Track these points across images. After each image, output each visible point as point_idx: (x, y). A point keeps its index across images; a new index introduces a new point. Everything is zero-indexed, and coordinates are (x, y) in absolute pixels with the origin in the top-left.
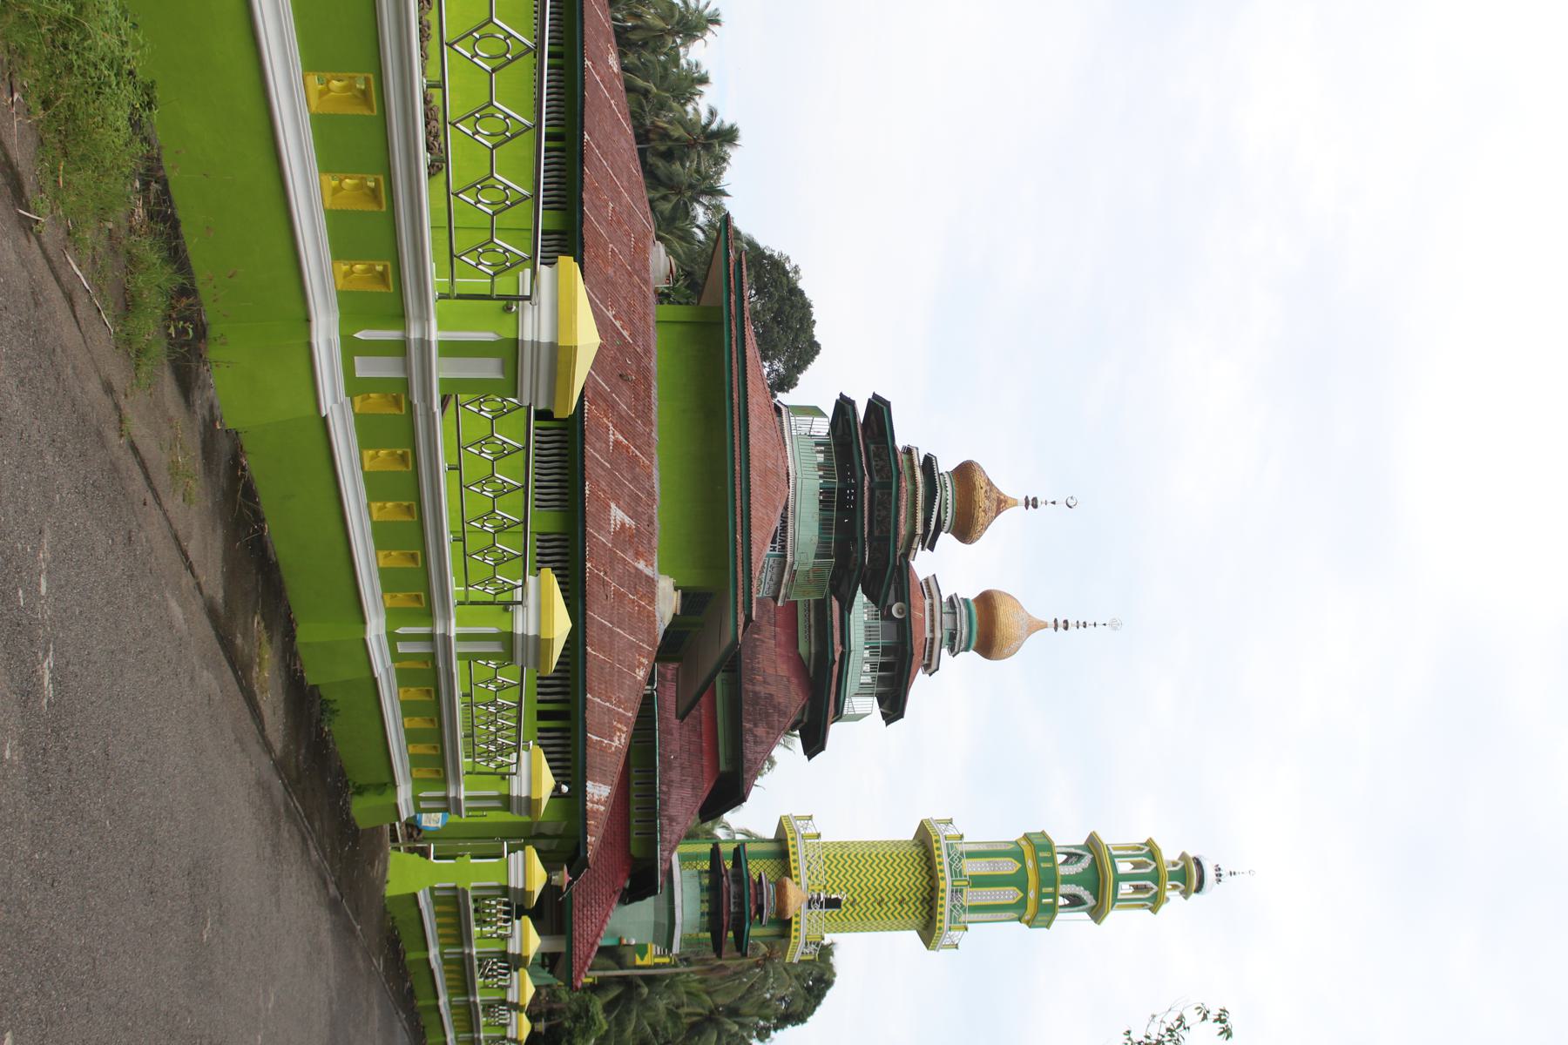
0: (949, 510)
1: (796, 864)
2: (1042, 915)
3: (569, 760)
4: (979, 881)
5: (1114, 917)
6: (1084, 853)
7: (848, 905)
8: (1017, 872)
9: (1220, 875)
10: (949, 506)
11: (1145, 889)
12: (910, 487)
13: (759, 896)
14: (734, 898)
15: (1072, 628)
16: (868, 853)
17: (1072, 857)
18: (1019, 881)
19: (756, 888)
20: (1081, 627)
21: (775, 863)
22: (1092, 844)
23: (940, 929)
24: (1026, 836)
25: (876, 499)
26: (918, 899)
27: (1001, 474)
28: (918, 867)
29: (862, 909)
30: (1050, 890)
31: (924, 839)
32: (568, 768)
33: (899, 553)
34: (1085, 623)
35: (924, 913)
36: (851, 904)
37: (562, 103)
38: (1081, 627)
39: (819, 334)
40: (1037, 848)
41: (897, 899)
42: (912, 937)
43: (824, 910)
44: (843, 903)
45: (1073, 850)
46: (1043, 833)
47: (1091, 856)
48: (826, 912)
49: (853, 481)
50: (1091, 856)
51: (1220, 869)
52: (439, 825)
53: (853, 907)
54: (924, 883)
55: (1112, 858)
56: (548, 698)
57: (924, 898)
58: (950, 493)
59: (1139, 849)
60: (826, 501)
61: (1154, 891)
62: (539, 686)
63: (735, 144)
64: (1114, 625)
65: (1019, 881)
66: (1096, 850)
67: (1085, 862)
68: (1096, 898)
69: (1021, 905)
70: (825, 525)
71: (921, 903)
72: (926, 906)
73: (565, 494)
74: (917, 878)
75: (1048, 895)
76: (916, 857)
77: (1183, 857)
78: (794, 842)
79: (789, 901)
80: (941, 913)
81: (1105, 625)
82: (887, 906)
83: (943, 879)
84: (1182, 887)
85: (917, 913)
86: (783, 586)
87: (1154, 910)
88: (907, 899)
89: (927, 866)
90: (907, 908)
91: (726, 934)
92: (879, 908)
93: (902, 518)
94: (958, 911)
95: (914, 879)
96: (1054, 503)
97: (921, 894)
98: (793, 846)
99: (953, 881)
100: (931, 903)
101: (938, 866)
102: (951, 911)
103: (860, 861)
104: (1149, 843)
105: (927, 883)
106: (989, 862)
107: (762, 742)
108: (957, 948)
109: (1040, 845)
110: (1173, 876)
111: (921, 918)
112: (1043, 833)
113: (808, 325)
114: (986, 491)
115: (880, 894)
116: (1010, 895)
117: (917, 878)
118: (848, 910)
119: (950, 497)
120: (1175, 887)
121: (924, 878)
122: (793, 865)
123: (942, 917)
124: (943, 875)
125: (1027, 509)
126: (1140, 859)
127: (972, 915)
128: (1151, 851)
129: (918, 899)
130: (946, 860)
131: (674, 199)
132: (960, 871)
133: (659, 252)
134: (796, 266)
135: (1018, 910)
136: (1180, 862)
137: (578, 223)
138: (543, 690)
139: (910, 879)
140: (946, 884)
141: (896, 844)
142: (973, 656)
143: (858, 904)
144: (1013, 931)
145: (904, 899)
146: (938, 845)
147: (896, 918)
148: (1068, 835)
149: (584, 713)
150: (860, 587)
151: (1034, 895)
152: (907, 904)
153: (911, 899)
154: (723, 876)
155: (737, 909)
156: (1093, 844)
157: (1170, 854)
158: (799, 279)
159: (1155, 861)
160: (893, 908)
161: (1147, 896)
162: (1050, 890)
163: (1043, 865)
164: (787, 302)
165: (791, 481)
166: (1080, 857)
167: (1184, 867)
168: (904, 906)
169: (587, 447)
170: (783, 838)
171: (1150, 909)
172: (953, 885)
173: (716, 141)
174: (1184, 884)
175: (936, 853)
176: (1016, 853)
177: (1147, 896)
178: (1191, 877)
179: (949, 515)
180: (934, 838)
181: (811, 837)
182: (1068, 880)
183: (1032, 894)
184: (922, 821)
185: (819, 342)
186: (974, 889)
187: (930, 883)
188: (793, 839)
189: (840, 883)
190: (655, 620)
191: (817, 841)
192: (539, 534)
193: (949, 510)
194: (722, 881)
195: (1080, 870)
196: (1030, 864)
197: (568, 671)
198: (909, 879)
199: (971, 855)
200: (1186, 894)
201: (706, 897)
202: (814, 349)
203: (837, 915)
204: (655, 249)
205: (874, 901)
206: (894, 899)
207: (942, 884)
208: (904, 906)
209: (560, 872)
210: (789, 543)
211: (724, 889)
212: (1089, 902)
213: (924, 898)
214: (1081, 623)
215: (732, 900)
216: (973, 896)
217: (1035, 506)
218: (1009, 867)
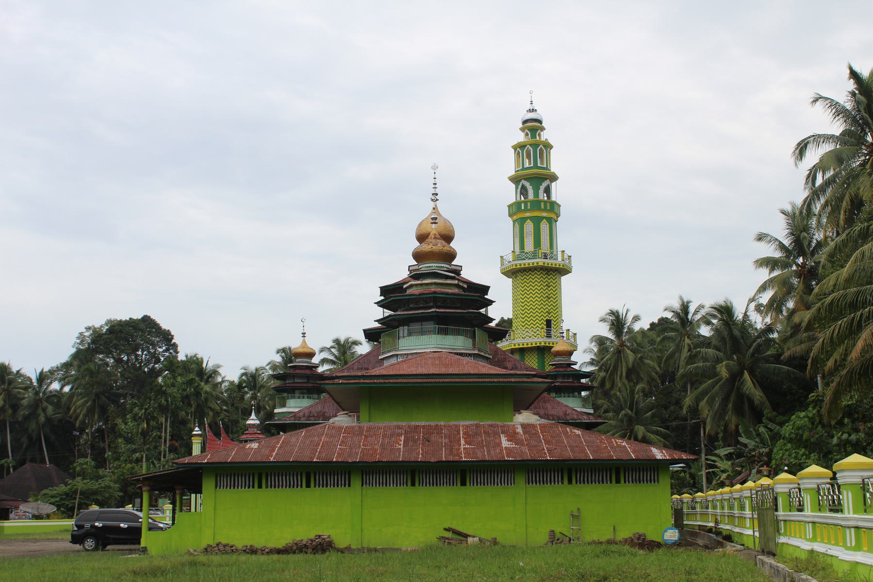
0: (442, 265)
1: (530, 344)
2: (553, 208)
3: (639, 468)
4: (537, 243)
5: (554, 168)
6: (521, 184)
7: (550, 316)
8: (532, 222)
9: (533, 109)
10: (440, 265)
11: (541, 151)
12: (433, 286)
13: (562, 366)
14: (565, 379)
15: (437, 191)
16: (521, 303)
17: (524, 191)
18: (537, 221)
19: (559, 367)
20: (436, 186)
21: (527, 355)
22: (515, 179)
23: (563, 266)
24: (510, 215)
25: (442, 305)
26: (547, 277)
28: (529, 277)
30: (542, 204)
31: (511, 273)
32: (643, 468)
33: (463, 293)
34: (434, 184)
35: (554, 274)
36: (549, 314)
37: (288, 473)
38: (436, 186)
39: (138, 315)
40: (519, 210)
41: (546, 289)
42: (564, 279)
43: (552, 329)
44: (549, 318)
45: (519, 190)
46: (509, 206)
47: (523, 181)
48: (553, 327)
50: (523, 181)
51: (530, 110)
52: (677, 531)
53: (551, 313)
54: (539, 274)
55: (524, 169)
56: (299, 483)
57: (546, 273)
58: (433, 265)
59: (519, 153)
60: (444, 332)
61: (542, 147)
62: (249, 488)
63: (8, 364)
64: (435, 168)
65: (537, 221)
66: (520, 177)
67: (527, 184)
68: (546, 179)
70: (457, 333)
71: (549, 276)
72: (550, 273)
73: (379, 471)
74: (536, 277)
76: (524, 277)
77: (522, 130)
78: (517, 344)
79: (566, 349)
80: (552, 264)
81: (435, 173)
82: (550, 294)
83: (537, 263)
84: (539, 131)
85: (554, 278)
86: (480, 353)
87: (551, 147)
88: (547, 283)
89: (534, 271)
90: (551, 283)
91: (582, 383)
92: (551, 299)
93: (450, 291)
95: (536, 279)
97: (544, 275)
98: (519, 345)
100: (549, 270)
103: (526, 308)
104: (515, 148)
105: (527, 272)
106: (526, 238)
107: (515, 364)
108: (571, 256)
109: (514, 209)
110: (534, 136)
111: (556, 276)
112: (509, 206)
113: (134, 322)
114: (433, 245)
115: (544, 298)
116: (544, 226)
117: (536, 277)
118: (552, 316)
119: (436, 265)
120: (539, 135)
121: (536, 273)
122: (529, 346)
123: (554, 264)
124: (531, 263)
126: (525, 154)
127: (554, 248)
128: (519, 148)
129: (547, 277)
130: (527, 261)
131: (45, 404)
132: (533, 253)
133: (338, 421)
134: (86, 328)
135: (552, 222)
136: (525, 132)
137: (364, 464)
138: (343, 485)
139: (536, 281)
140: (540, 262)
141: (514, 287)
143: (549, 310)
144: (561, 225)
145: (547, 285)
146: (518, 265)
147: (556, 289)
148: (510, 193)
149: (624, 460)
151: (544, 213)
152: (549, 283)
153: (547, 281)
154: (555, 385)
155: (571, 378)
156: (515, 180)
157: (521, 137)
158: (94, 327)
159: (526, 146)
160: (552, 291)
161: (545, 151)
162: (542, 204)
163: (529, 208)
164: (119, 335)
165: (438, 350)
166: (523, 187)
167: (528, 130)
168: (550, 285)
169: (248, 460)
170: (511, 350)
171: (550, 149)
172: (541, 258)
173: (6, 378)
174: (538, 130)
175: (523, 266)
176: (520, 223)
177: (545, 151)
178: (533, 126)
179: (444, 265)
180: (514, 267)
182: (536, 194)
183: (545, 214)
184: (502, 273)
185: (142, 316)
186: (542, 245)
187: (538, 270)
188: (515, 345)
189: (539, 320)
190: (543, 424)
192: (362, 486)
193: (442, 265)
194: (557, 386)
195: (531, 187)
196: (528, 215)
197: (595, 469)
198: (536, 282)
199: (522, 246)
200: (543, 129)
201: (566, 395)
202: (146, 319)
203: (555, 322)
204: (337, 423)
205: (548, 301)
206: (547, 290)
207: (541, 264)
208: (550, 285)
209: (763, 471)
210: (468, 352)
211: (562, 385)
212: (548, 183)
213: (546, 273)
214: (434, 186)
215: (566, 380)
217: (305, 333)
218: (529, 227)
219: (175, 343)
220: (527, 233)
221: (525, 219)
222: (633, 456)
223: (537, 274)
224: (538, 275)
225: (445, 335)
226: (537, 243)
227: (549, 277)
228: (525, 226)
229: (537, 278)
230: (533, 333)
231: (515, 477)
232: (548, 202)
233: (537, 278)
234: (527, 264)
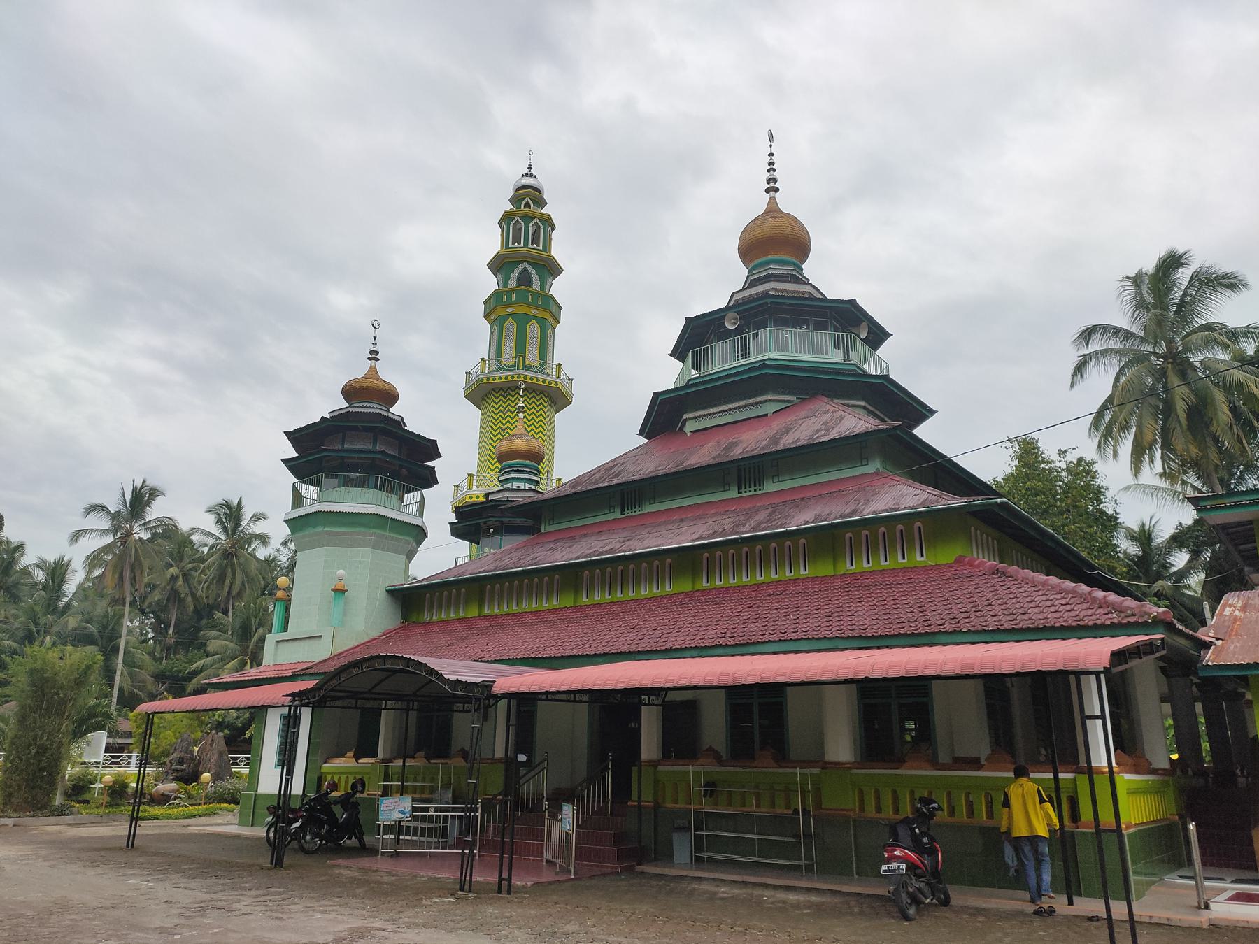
4: (521, 350)
18: (523, 320)
27: (358, 370)
29: (537, 417)
47: (525, 264)
50: (525, 264)
65: (523, 320)
69: (542, 322)
74: (501, 400)
75: (535, 299)
89: (540, 393)
96: (375, 338)
116: (533, 330)
125: (379, 360)
142: (810, 269)
172: (523, 369)
183: (535, 312)
191: (475, 477)
196: (510, 310)
216: (532, 356)
217: (377, 353)
218: (511, 327)
221: (504, 318)
224: (512, 396)
226: (521, 350)
229: (536, 398)
230: (489, 477)
231: (399, 711)
233: (536, 398)
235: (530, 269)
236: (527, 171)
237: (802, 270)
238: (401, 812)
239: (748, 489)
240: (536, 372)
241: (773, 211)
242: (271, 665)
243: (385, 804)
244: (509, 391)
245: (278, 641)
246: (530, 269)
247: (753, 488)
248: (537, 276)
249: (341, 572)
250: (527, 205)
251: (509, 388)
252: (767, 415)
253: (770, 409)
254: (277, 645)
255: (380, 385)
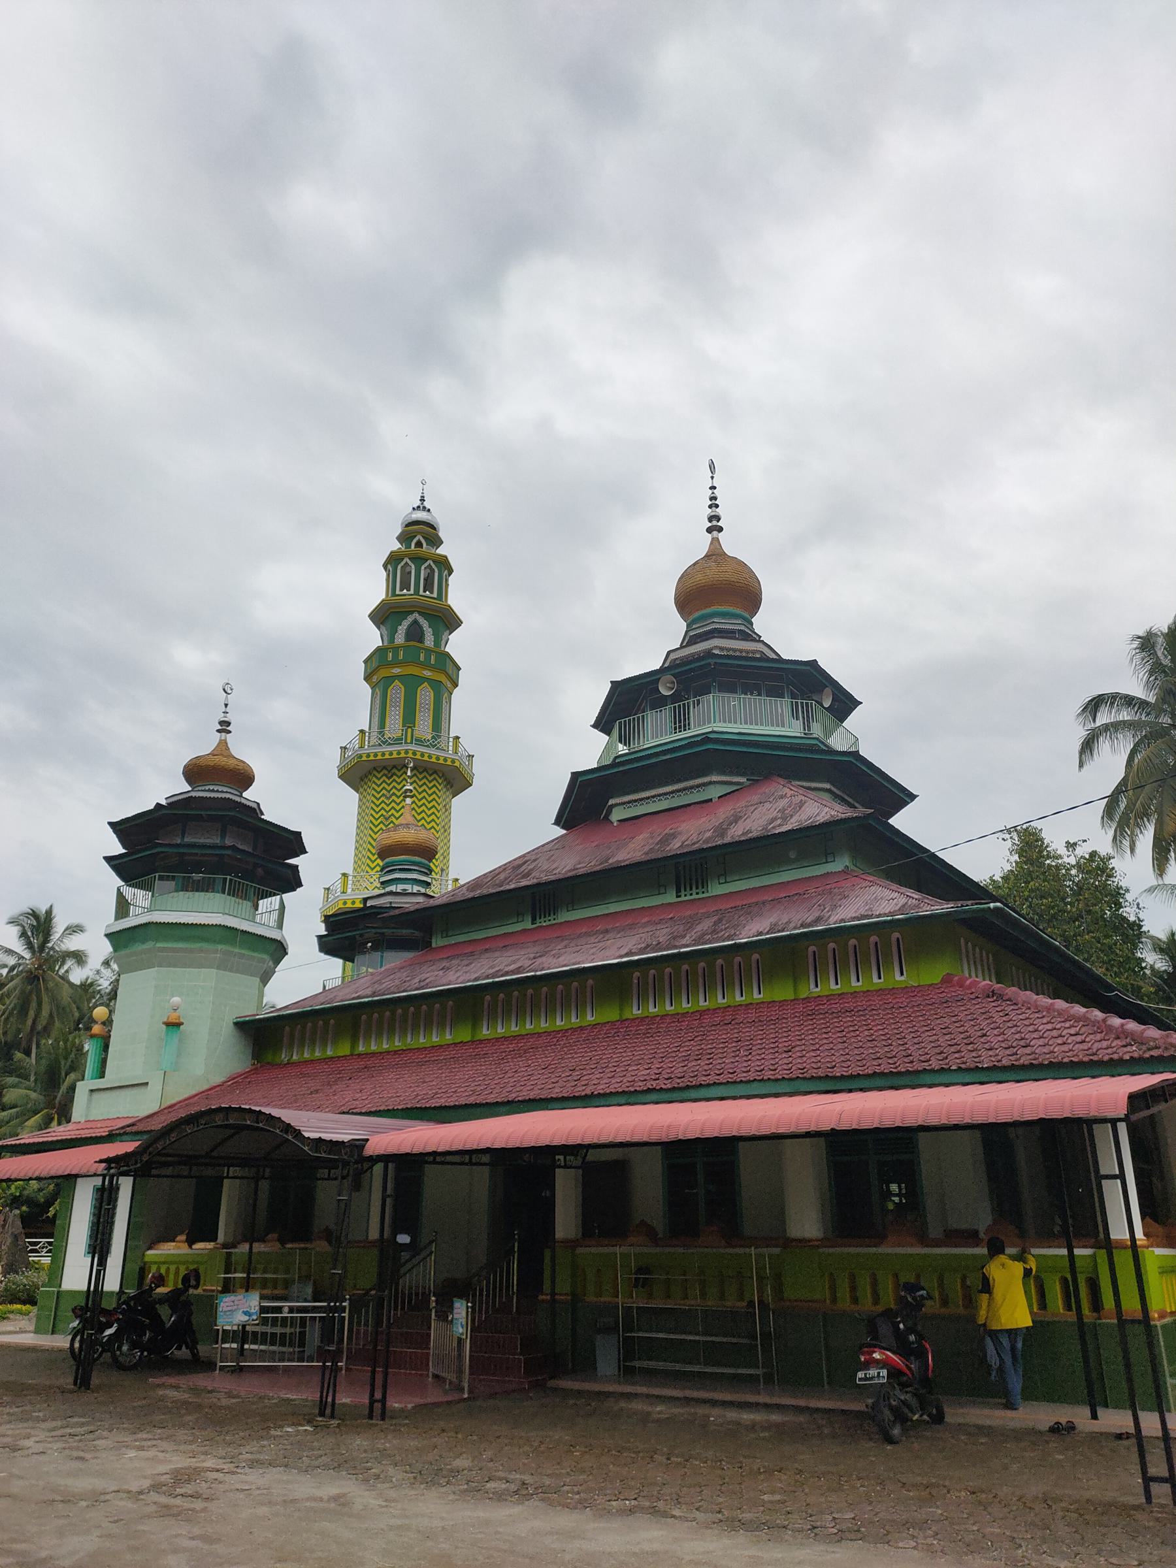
4: (409, 719)
27: (204, 745)
39: (293, 827)
47: (416, 615)
49: (370, 944)
50: (416, 615)
69: (436, 686)
75: (428, 658)
76: (381, 780)
89: (423, 772)
94: (438, 743)
96: (226, 705)
99: (406, 743)
101: (385, 757)
102: (437, 748)
105: (399, 777)
116: (425, 695)
142: (761, 623)
150: (287, 861)
151: (427, 671)
159: (427, 560)
161: (436, 570)
163: (401, 657)
172: (412, 743)
177: (436, 570)
181: (345, 885)
183: (427, 673)
191: (350, 878)
196: (396, 671)
199: (382, 725)
216: (423, 728)
217: (229, 724)
219: (295, 868)
220: (429, 710)
222: (241, 1275)
223: (427, 779)
225: (241, 898)
227: (430, 785)
228: (389, 692)
232: (434, 652)
234: (372, 755)
235: (425, 624)
236: (418, 503)
237: (752, 624)
238: (245, 1313)
239: (688, 892)
240: (427, 746)
241: (715, 554)
242: (83, 1121)
243: (226, 1303)
244: (394, 770)
245: (92, 1091)
246: (425, 624)
247: (694, 891)
248: (430, 630)
249: (176, 1000)
250: (419, 544)
251: (394, 767)
252: (711, 800)
253: (714, 792)
254: (91, 1095)
255: (231, 763)
